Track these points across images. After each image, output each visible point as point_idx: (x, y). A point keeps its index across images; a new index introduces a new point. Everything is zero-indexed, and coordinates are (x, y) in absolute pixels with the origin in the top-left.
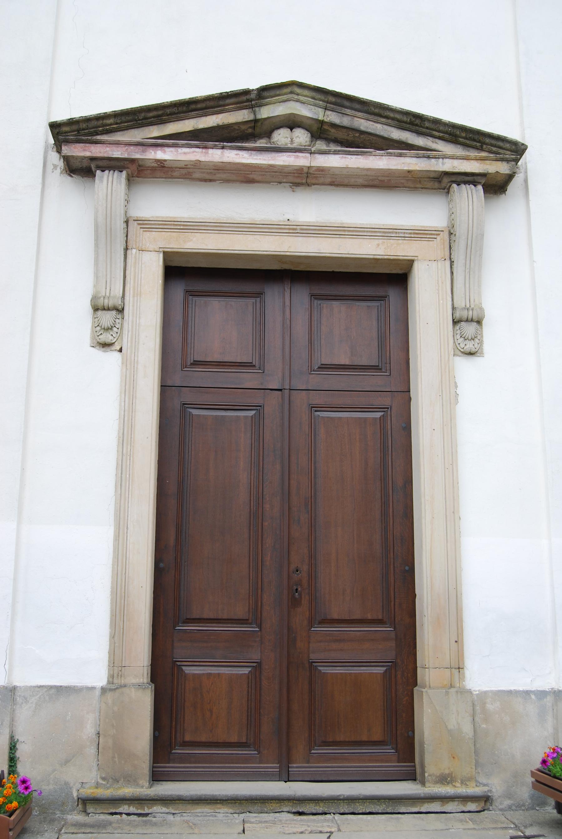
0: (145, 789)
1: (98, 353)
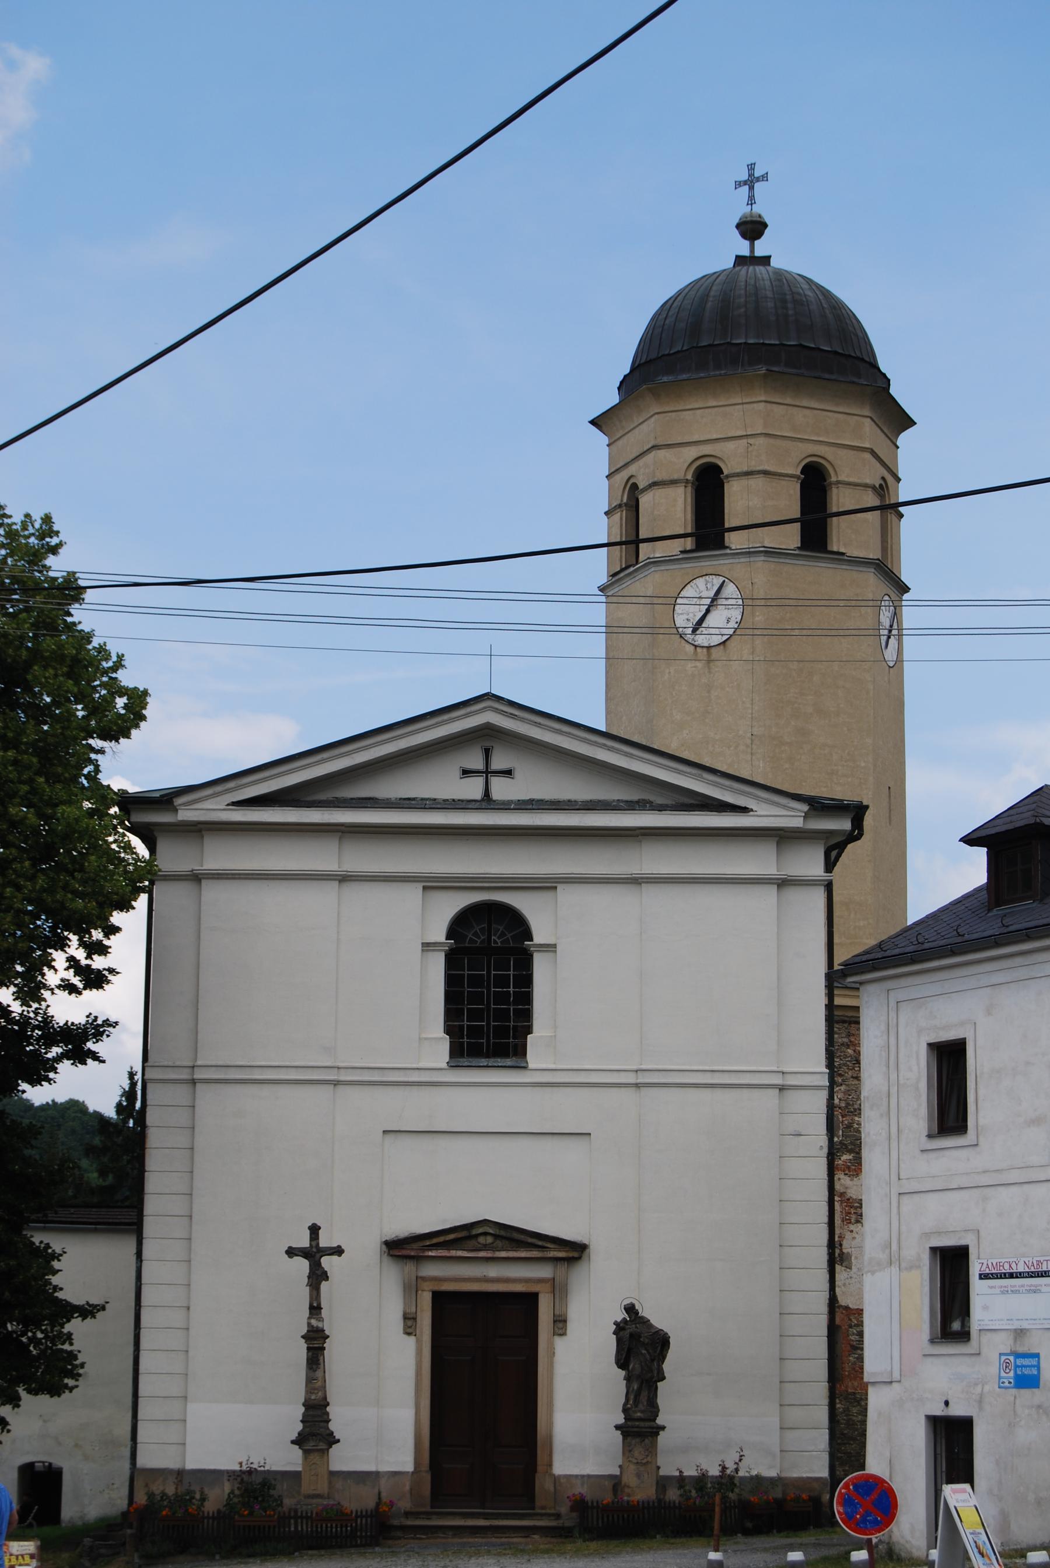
0: (428, 1509)
1: (406, 1336)
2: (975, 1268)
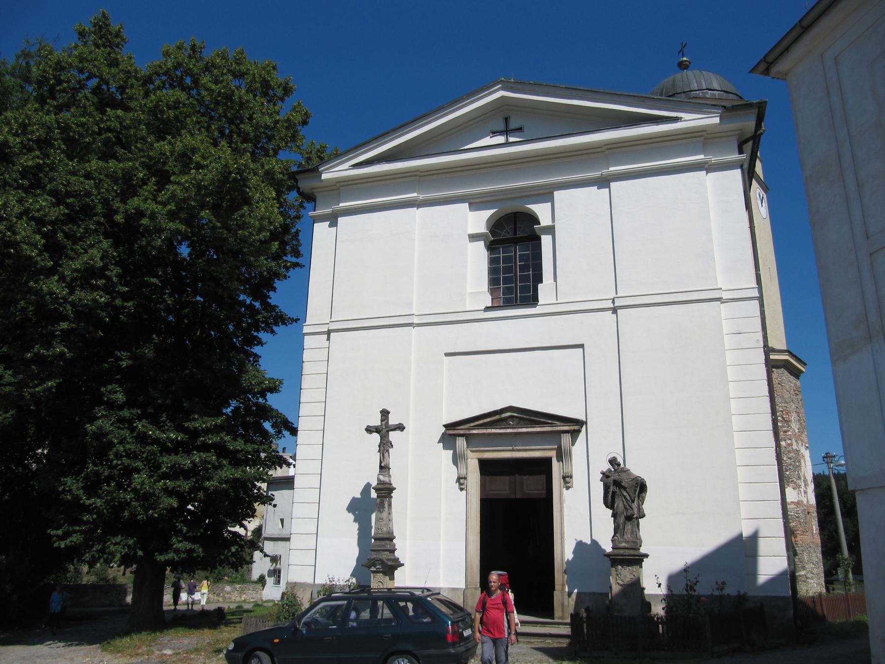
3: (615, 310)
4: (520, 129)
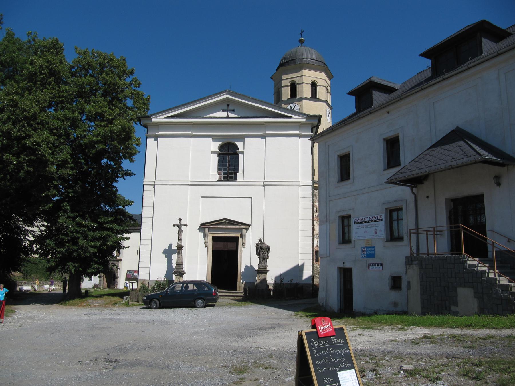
2: (353, 220)
3: (264, 186)
4: (233, 110)
